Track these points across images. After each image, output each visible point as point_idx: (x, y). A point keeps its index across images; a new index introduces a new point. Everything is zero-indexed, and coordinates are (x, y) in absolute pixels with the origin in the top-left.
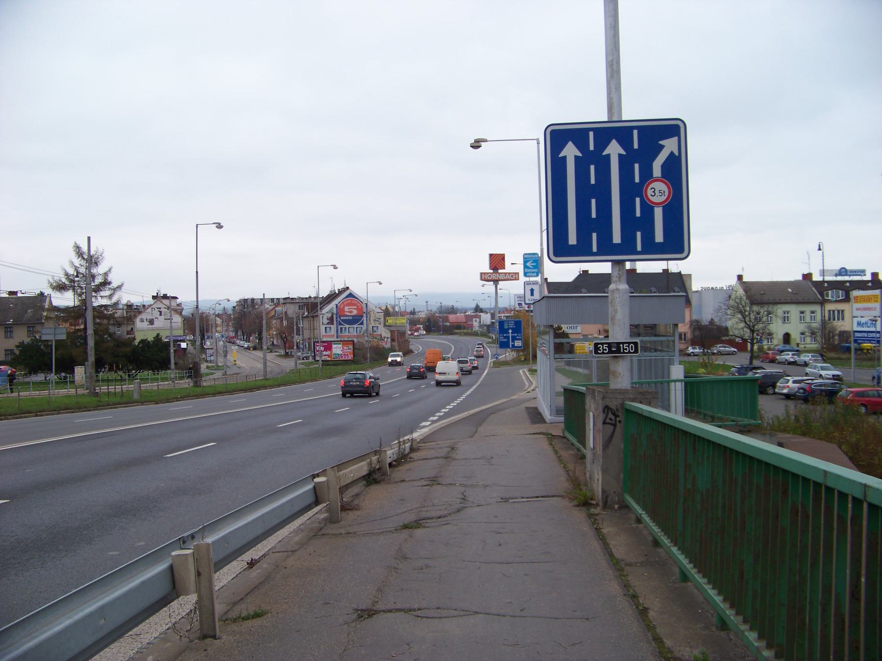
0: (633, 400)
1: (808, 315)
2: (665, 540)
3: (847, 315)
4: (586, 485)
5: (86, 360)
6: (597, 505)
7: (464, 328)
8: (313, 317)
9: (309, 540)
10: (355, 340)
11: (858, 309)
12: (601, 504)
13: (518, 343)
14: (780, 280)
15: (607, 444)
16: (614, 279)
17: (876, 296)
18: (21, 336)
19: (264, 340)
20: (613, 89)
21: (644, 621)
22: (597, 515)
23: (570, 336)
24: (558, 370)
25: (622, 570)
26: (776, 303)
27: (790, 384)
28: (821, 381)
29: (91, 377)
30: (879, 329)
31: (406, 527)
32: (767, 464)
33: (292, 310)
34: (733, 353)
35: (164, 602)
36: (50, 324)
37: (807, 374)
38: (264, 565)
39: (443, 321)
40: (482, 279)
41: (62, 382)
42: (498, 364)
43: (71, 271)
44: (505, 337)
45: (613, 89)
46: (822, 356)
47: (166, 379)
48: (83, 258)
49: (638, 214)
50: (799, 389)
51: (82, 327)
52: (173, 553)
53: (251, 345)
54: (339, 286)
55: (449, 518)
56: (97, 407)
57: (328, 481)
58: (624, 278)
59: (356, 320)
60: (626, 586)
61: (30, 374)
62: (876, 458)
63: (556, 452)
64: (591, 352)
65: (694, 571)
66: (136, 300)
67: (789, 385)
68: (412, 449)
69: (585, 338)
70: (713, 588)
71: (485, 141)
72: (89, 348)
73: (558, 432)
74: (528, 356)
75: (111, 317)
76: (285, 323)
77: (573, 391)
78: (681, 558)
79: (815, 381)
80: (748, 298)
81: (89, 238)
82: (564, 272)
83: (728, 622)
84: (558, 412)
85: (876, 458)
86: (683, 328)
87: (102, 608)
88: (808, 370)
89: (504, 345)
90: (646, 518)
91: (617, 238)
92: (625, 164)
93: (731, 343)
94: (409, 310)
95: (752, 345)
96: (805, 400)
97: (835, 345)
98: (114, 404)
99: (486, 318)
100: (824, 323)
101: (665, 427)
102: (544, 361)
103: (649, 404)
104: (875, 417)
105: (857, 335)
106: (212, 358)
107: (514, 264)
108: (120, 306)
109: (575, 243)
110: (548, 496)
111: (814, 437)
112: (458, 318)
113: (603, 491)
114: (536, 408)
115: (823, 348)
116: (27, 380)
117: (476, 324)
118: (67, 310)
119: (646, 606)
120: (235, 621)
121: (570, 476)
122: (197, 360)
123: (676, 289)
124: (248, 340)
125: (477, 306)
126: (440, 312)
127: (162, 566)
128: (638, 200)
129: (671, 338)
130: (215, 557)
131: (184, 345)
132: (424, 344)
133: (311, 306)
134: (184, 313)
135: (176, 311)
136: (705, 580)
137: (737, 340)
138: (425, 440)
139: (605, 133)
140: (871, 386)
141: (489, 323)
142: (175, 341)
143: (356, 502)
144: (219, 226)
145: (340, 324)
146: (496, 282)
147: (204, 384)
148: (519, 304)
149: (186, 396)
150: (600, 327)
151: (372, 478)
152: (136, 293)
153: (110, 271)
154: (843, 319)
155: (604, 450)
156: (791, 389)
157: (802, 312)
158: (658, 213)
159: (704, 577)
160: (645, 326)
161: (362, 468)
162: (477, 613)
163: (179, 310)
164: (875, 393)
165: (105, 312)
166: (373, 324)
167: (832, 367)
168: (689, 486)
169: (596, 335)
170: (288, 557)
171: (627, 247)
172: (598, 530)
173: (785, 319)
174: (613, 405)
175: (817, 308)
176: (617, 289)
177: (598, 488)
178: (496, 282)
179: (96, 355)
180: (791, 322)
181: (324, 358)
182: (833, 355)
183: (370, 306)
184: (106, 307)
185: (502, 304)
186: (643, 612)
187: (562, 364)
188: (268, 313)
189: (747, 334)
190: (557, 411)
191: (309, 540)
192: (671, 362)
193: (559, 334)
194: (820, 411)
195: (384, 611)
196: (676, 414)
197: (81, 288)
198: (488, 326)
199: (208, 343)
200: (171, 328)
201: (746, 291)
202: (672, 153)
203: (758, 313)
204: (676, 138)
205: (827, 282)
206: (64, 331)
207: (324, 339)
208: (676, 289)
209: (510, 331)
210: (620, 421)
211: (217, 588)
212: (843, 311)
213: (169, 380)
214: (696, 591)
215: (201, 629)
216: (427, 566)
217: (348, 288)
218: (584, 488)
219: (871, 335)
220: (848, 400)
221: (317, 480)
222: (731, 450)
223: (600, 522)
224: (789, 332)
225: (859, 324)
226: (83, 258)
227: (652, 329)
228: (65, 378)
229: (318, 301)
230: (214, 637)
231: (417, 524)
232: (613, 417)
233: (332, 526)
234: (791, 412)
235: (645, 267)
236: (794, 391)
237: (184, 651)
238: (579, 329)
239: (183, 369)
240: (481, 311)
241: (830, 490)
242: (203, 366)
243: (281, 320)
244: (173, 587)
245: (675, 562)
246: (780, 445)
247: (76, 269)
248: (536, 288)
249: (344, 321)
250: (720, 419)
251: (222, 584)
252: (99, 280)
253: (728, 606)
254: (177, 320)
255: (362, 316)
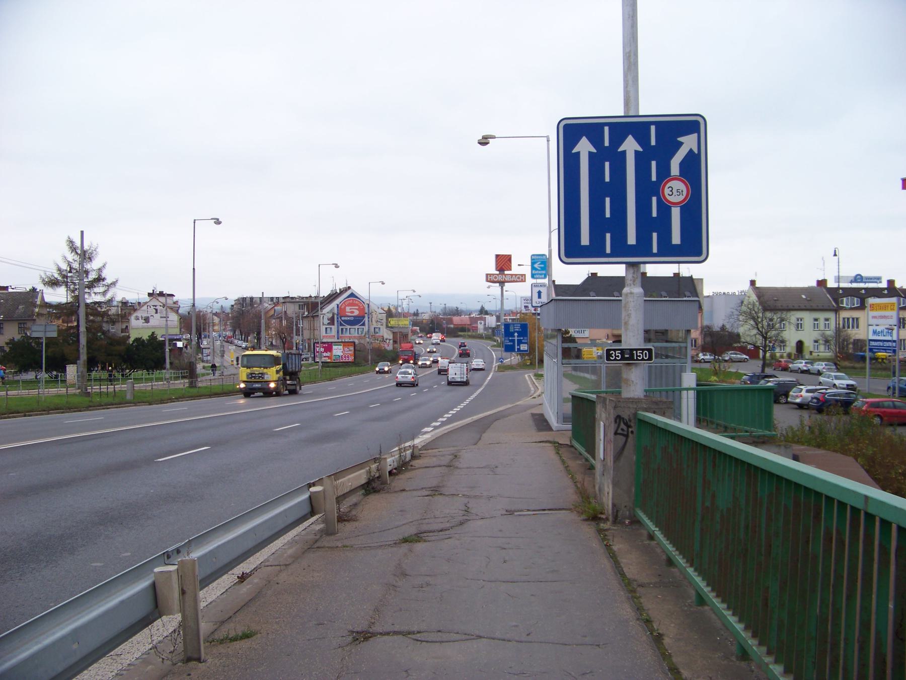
0: (646, 410)
1: (822, 323)
2: (680, 560)
3: (862, 323)
4: (595, 497)
5: (78, 358)
6: (607, 519)
7: (469, 331)
8: (313, 317)
9: (303, 553)
10: (357, 341)
11: (874, 317)
12: (611, 518)
13: (524, 347)
14: (793, 286)
15: (618, 456)
16: (628, 282)
17: (893, 304)
18: (12, 333)
19: (263, 340)
20: (630, 82)
21: (659, 648)
22: (606, 530)
23: (577, 340)
24: (566, 375)
25: (633, 591)
26: (789, 310)
27: (804, 393)
28: (835, 390)
29: (83, 377)
30: (895, 338)
31: (405, 540)
32: (797, 486)
33: (292, 310)
34: (744, 361)
35: (146, 622)
36: (41, 321)
37: (820, 383)
38: (255, 580)
39: (447, 323)
40: (487, 281)
41: (54, 381)
42: (503, 368)
43: (64, 267)
44: (510, 341)
45: (630, 82)
46: (836, 364)
47: (161, 379)
48: (77, 253)
49: (654, 214)
50: (813, 398)
51: (75, 324)
52: (156, 570)
53: (249, 345)
54: (341, 286)
55: (451, 531)
56: (88, 408)
57: (324, 491)
58: (639, 281)
59: (357, 321)
60: (639, 609)
61: (20, 371)
62: (893, 473)
63: (563, 462)
64: (600, 357)
65: (712, 595)
66: (132, 297)
67: (802, 394)
68: (413, 457)
69: (594, 343)
70: (733, 615)
71: (493, 137)
72: (81, 346)
73: (565, 440)
74: (534, 360)
75: (105, 314)
76: (284, 323)
77: (582, 399)
78: (698, 579)
79: (829, 391)
80: (761, 303)
81: (82, 232)
82: (573, 274)
83: (749, 652)
84: (565, 420)
85: (893, 473)
86: (695, 334)
87: (75, 631)
88: (821, 379)
89: (509, 349)
90: (659, 534)
91: (632, 240)
92: (642, 161)
93: (743, 350)
94: (412, 311)
95: (765, 352)
96: (820, 410)
97: (850, 354)
98: (106, 405)
99: (491, 321)
100: (838, 331)
101: (680, 439)
102: (552, 365)
103: (663, 414)
104: (891, 428)
105: (873, 343)
106: (209, 358)
107: (521, 265)
108: (115, 303)
109: (634, 243)
110: (556, 510)
111: (829, 450)
112: (463, 320)
113: (614, 505)
114: (542, 415)
115: (837, 356)
116: (17, 378)
117: (480, 327)
118: (59, 306)
119: (660, 632)
120: (222, 641)
121: (578, 488)
122: (193, 360)
123: (687, 293)
124: (246, 340)
125: (482, 308)
126: (445, 314)
127: (144, 584)
128: (654, 199)
129: (682, 345)
130: (201, 573)
131: (180, 344)
132: (429, 347)
133: (312, 306)
134: (181, 311)
135: (171, 308)
136: (725, 606)
137: (749, 347)
138: (427, 446)
139: (621, 129)
140: (886, 397)
141: (494, 325)
142: (171, 340)
143: (354, 513)
144: (218, 222)
145: (341, 325)
146: (502, 283)
147: (200, 385)
148: (526, 307)
149: (181, 397)
150: (608, 331)
151: (371, 487)
152: (130, 289)
153: (104, 266)
154: (858, 327)
155: (614, 462)
156: (804, 399)
157: (816, 320)
158: (676, 213)
159: (723, 602)
160: (656, 332)
161: (360, 477)
162: (480, 637)
163: (175, 308)
164: (891, 403)
165: (99, 309)
166: (375, 325)
167: (846, 377)
168: (708, 504)
169: (604, 340)
170: (280, 571)
171: (643, 249)
172: (608, 547)
173: (799, 326)
174: (626, 415)
175: (831, 315)
176: (631, 293)
177: (608, 502)
178: (502, 283)
179: (88, 353)
180: (805, 330)
181: (324, 359)
182: (847, 364)
183: (372, 307)
184: (99, 303)
185: (508, 306)
186: (658, 639)
187: (569, 369)
188: (267, 312)
189: (759, 341)
190: (564, 418)
191: (303, 553)
192: (682, 370)
193: (568, 339)
194: (835, 422)
195: (381, 634)
196: (686, 423)
197: (74, 284)
198: (493, 329)
199: (205, 343)
200: (167, 327)
201: (759, 297)
202: (691, 151)
203: (771, 320)
204: (696, 135)
205: (842, 289)
206: (56, 328)
207: (325, 340)
208: (687, 293)
209: (516, 334)
210: (632, 432)
211: (202, 605)
212: (857, 319)
213: (165, 381)
214: (713, 616)
215: (185, 651)
216: (428, 584)
217: (349, 288)
218: (592, 501)
219: (887, 344)
220: (864, 411)
221: (313, 489)
222: (756, 468)
223: (610, 538)
224: (803, 339)
225: (875, 332)
226: (77, 253)
227: (662, 335)
228: (57, 376)
229: (319, 301)
230: (199, 660)
231: (417, 538)
232: (625, 428)
233: (328, 538)
234: (805, 423)
235: (654, 270)
236: (806, 401)
237: (166, 675)
238: (587, 334)
239: (178, 369)
240: (487, 313)
241: (870, 517)
242: (199, 367)
243: (281, 319)
244: (154, 606)
245: (691, 584)
246: (796, 458)
247: (69, 264)
248: (544, 291)
249: (345, 321)
250: (734, 430)
251: (210, 600)
252: (92, 276)
253: (750, 634)
254: (174, 318)
255: (364, 317)
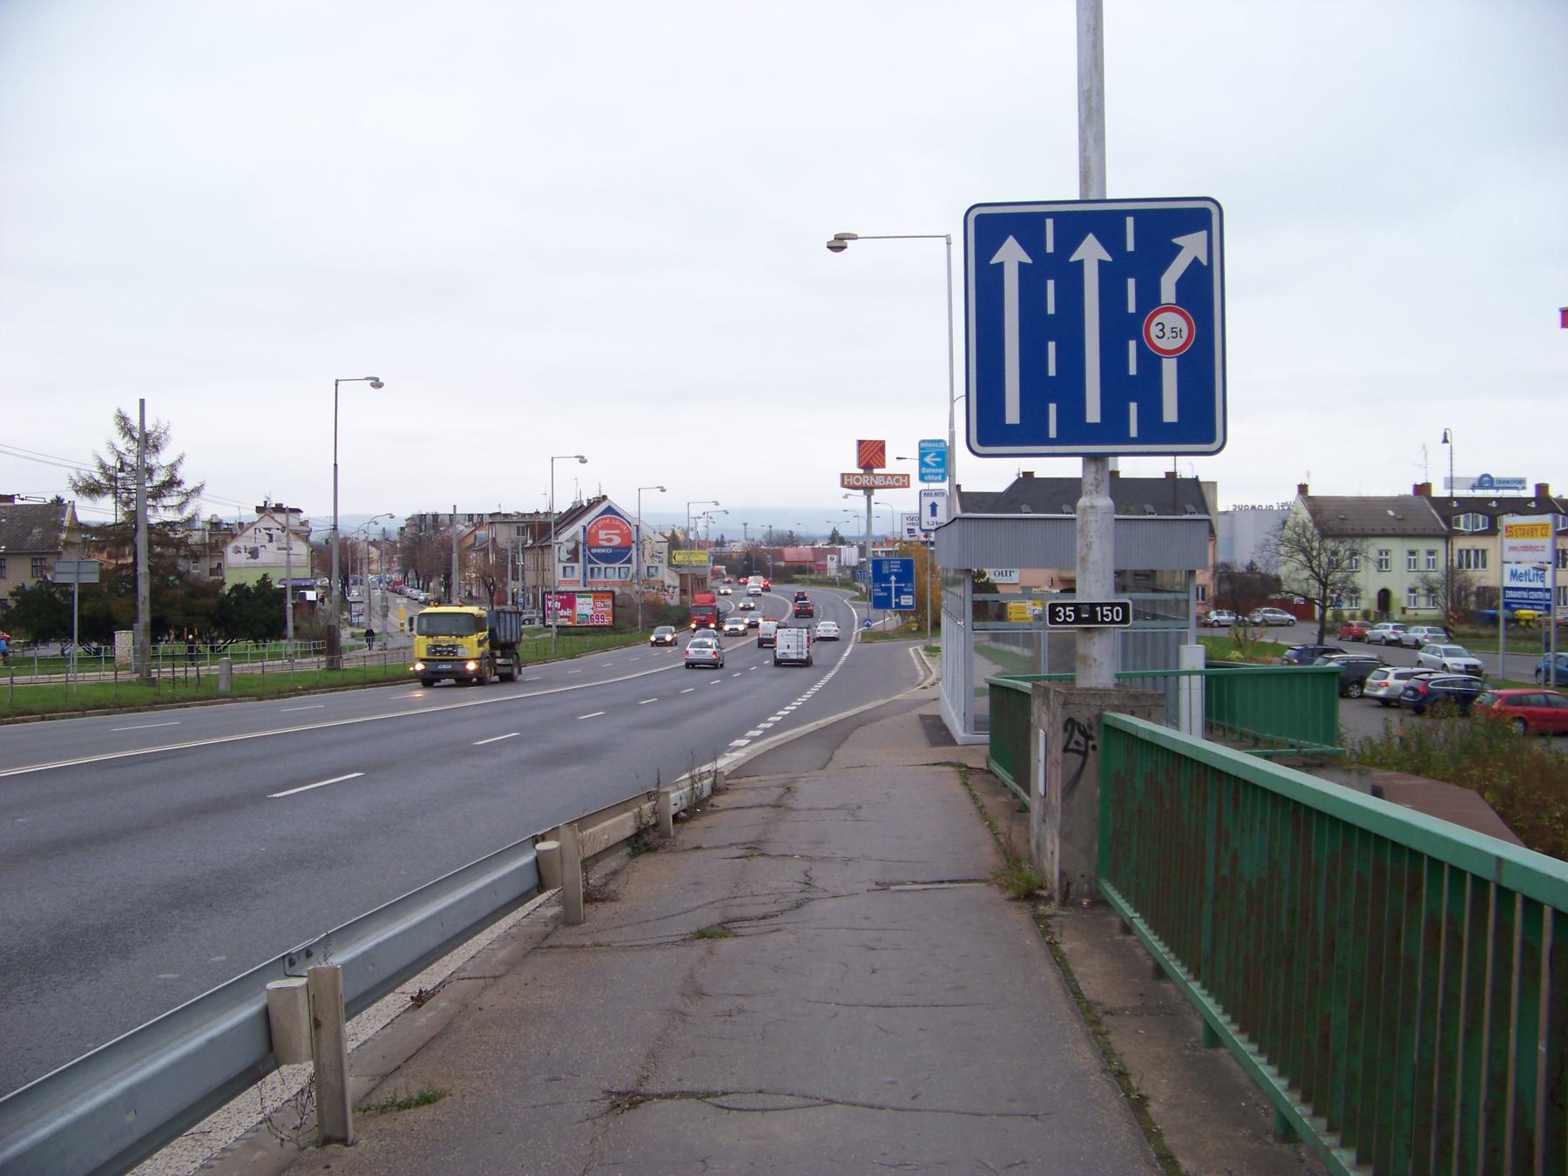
0: (1119, 709)
1: (1422, 558)
2: (1178, 969)
3: (1492, 559)
4: (1030, 860)
5: (135, 619)
6: (1051, 898)
7: (811, 572)
8: (542, 548)
9: (525, 956)
10: (617, 590)
11: (1512, 549)
12: (1057, 896)
13: (907, 600)
14: (1372, 494)
15: (1069, 789)
16: (1087, 487)
17: (1545, 526)
18: (20, 575)
19: (455, 588)
20: (1091, 142)
21: (1140, 1121)
22: (1049, 917)
23: (999, 588)
24: (979, 649)
25: (1096, 1022)
26: (1365, 536)
27: (1391, 680)
28: (1445, 675)
29: (143, 651)
30: (1549, 585)
31: (701, 935)
32: (1380, 840)
33: (505, 535)
34: (1287, 624)
35: (252, 1075)
36: (72, 556)
37: (1419, 663)
38: (441, 1003)
39: (774, 559)
40: (843, 485)
41: (94, 659)
42: (870, 636)
43: (111, 461)
44: (883, 590)
45: (1091, 142)
46: (1446, 630)
47: (278, 656)
48: (133, 438)
49: (1133, 371)
50: (1406, 689)
51: (130, 560)
52: (271, 985)
53: (430, 596)
54: (589, 494)
55: (781, 919)
56: (152, 705)
57: (561, 849)
58: (1105, 485)
59: (618, 555)
60: (1106, 1053)
61: (35, 642)
62: (1546, 818)
63: (975, 799)
64: (1039, 618)
65: (1232, 1029)
66: (228, 514)
67: (1389, 681)
68: (715, 790)
69: (1027, 593)
70: (1269, 1063)
71: (854, 237)
72: (141, 599)
73: (977, 762)
74: (924, 623)
75: (182, 543)
76: (492, 558)
77: (1007, 689)
78: (1208, 1002)
79: (1434, 676)
80: (1317, 525)
81: (142, 402)
82: (991, 474)
83: (1297, 1127)
84: (978, 726)
85: (1546, 818)
86: (1203, 578)
87: (130, 1092)
88: (1422, 655)
89: (881, 603)
90: (1140, 924)
91: (1093, 414)
92: (1111, 278)
93: (1286, 605)
94: (713, 538)
95: (1324, 608)
96: (1418, 709)
97: (1471, 613)
98: (184, 700)
99: (850, 555)
100: (1450, 572)
101: (1178, 760)
102: (955, 631)
103: (1148, 716)
104: (1543, 741)
105: (1510, 594)
106: (362, 619)
107: (901, 458)
108: (199, 525)
109: (1098, 420)
110: (962, 881)
111: (1434, 778)
112: (801, 553)
113: (1062, 874)
114: (938, 718)
115: (1448, 616)
116: (29, 654)
117: (832, 565)
118: (102, 530)
119: (1143, 1092)
120: (384, 1109)
121: (1000, 843)
122: (334, 622)
123: (1189, 507)
124: (426, 589)
125: (835, 533)
126: (769, 543)
127: (250, 1009)
128: (1132, 345)
129: (1181, 596)
130: (347, 991)
131: (311, 595)
132: (743, 600)
133: (539, 529)
134: (312, 538)
135: (297, 533)
136: (1254, 1047)
137: (1297, 600)
138: (739, 772)
139: (1075, 223)
140: (1533, 686)
141: (854, 563)
142: (296, 588)
143: (612, 887)
144: (377, 384)
145: (591, 561)
146: (869, 490)
147: (346, 665)
148: (910, 531)
149: (313, 687)
150: (1053, 573)
151: (642, 842)
152: (226, 500)
153: (179, 461)
154: (1484, 566)
155: (1063, 799)
156: (1392, 689)
157: (1412, 553)
158: (1169, 368)
159: (1251, 1040)
160: (1136, 574)
161: (623, 825)
162: (831, 1102)
163: (303, 533)
164: (1542, 697)
165: (171, 534)
166: (649, 562)
167: (1465, 652)
168: (1225, 871)
169: (1046, 588)
170: (485, 987)
171: (1112, 431)
172: (1052, 945)
173: (1383, 565)
174: (1083, 717)
175: (1439, 546)
176: (1092, 507)
177: (1052, 868)
178: (869, 490)
179: (152, 611)
180: (1393, 571)
181: (560, 622)
182: (1465, 629)
183: (645, 531)
184: (172, 525)
185: (879, 529)
186: (1139, 1105)
187: (984, 638)
188: (462, 540)
189: (1314, 590)
190: (976, 723)
191: (525, 956)
192: (1181, 639)
193: (983, 586)
194: (1444, 730)
195: (659, 1096)
196: (1187, 732)
197: (129, 491)
198: (854, 569)
199: (355, 592)
200: (289, 565)
201: (1313, 513)
202: (1196, 261)
203: (1335, 553)
204: (1204, 233)
205: (1457, 499)
206: (96, 567)
207: (562, 589)
208: (1189, 507)
209: (893, 578)
210: (1094, 747)
211: (350, 1046)
212: (1484, 552)
213: (285, 658)
214: (1234, 1065)
215: (320, 1125)
216: (741, 1011)
217: (605, 497)
218: (1025, 866)
219: (1535, 595)
220: (1495, 711)
221: (541, 846)
222: (1309, 809)
223: (1056, 930)
224: (1389, 587)
225: (1514, 575)
226: (133, 438)
227: (1146, 579)
228: (98, 651)
229: (552, 520)
230: (344, 1141)
231: (721, 930)
232: (1082, 740)
233: (568, 931)
234: (1394, 731)
235: (1132, 467)
236: (1395, 694)
237: (288, 1168)
238: (1015, 577)
239: (308, 638)
240: (842, 541)
241: (1506, 894)
242: (345, 634)
243: (486, 551)
244: (267, 1048)
245: (1195, 1010)
246: (1377, 792)
247: (120, 456)
248: (941, 503)
249: (596, 555)
250: (1270, 743)
251: (363, 1038)
252: (160, 477)
253: (1298, 1097)
254: (301, 550)
255: (630, 548)
